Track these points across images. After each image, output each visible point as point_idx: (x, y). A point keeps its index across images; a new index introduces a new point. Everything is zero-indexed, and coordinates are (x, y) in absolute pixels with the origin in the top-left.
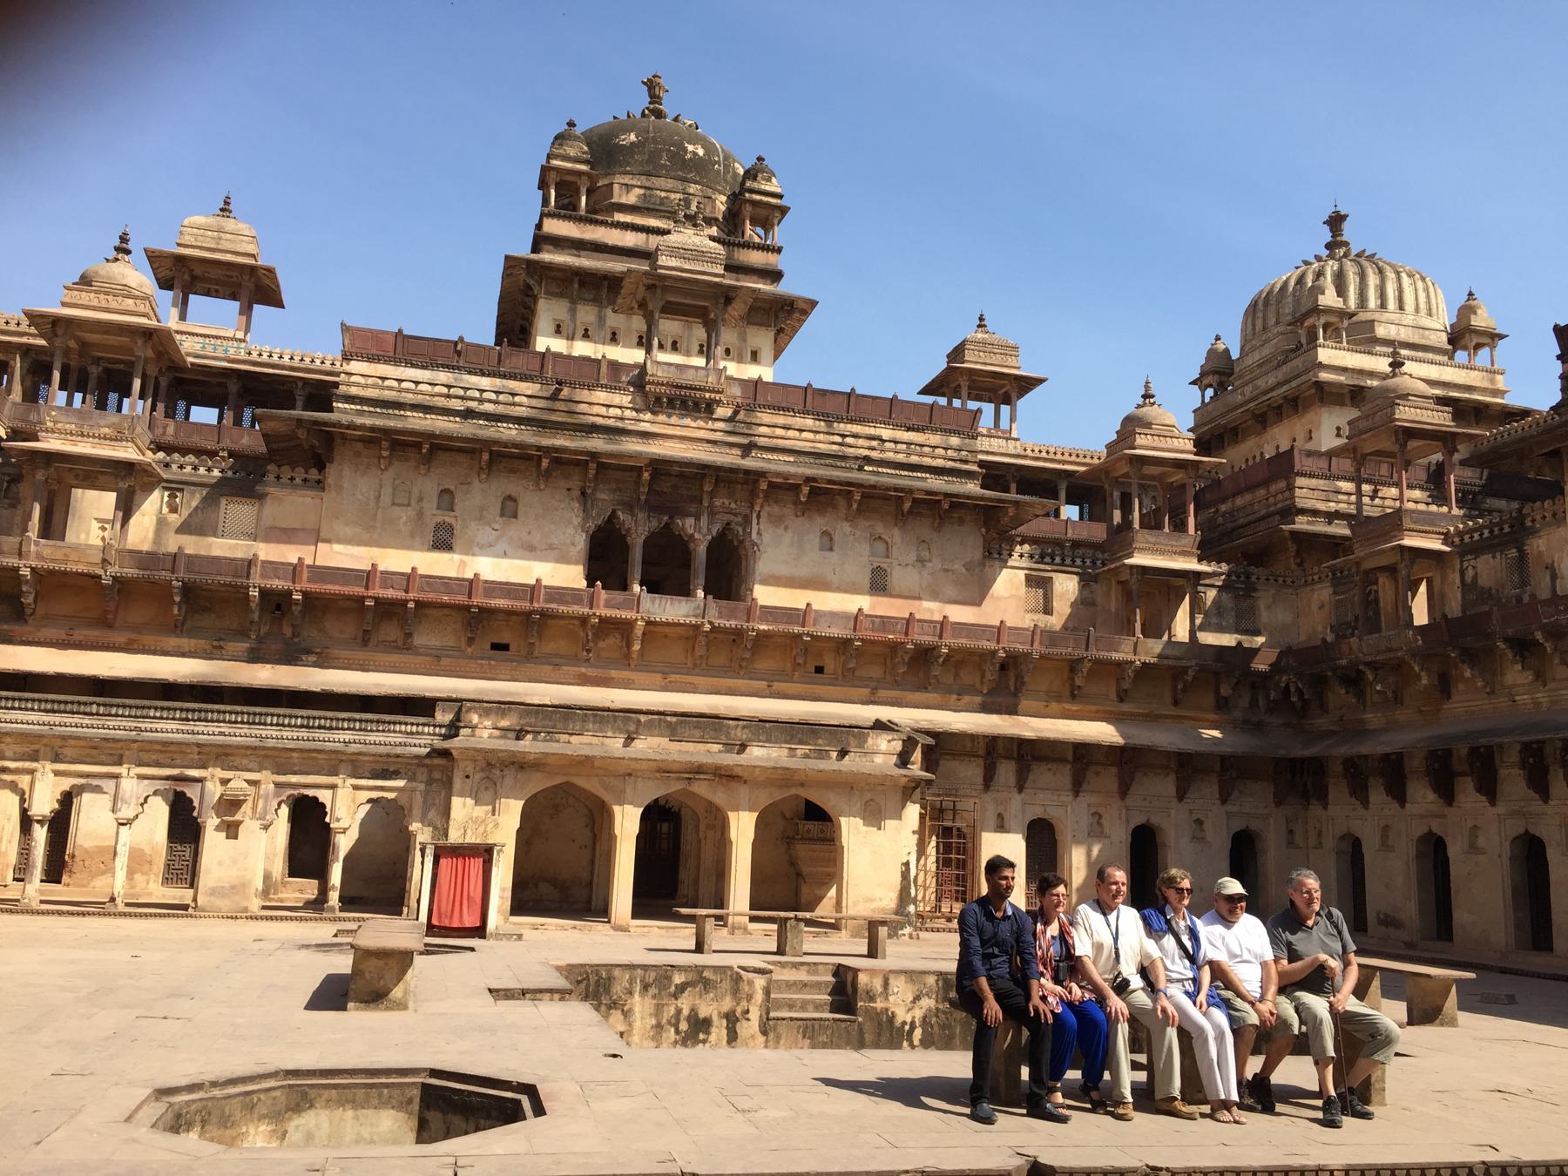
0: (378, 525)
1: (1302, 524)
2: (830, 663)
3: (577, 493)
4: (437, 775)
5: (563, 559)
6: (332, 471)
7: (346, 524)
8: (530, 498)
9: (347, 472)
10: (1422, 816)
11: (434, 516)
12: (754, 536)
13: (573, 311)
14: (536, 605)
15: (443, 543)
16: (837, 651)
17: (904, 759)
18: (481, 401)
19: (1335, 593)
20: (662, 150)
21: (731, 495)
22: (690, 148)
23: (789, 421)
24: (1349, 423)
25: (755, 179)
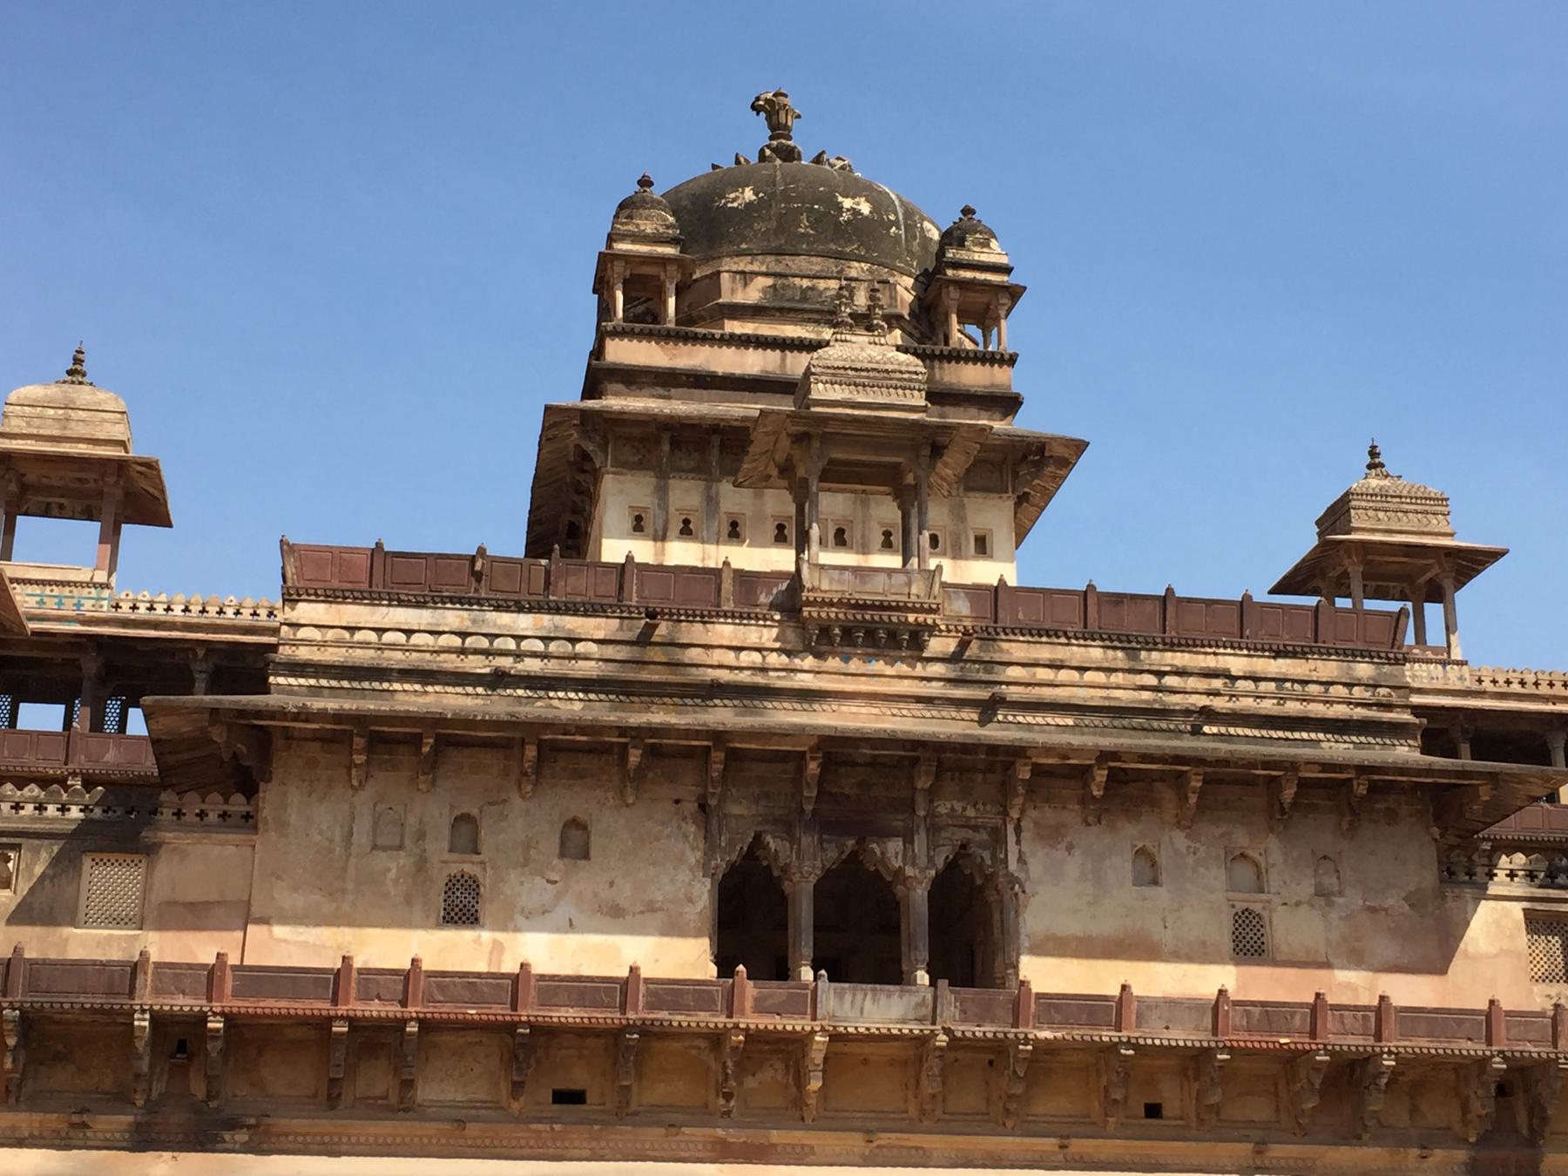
0: (350, 886)
3: (690, 807)
5: (674, 928)
6: (269, 795)
8: (611, 823)
9: (295, 797)
11: (445, 864)
12: (1013, 865)
13: (662, 492)
14: (631, 1015)
15: (461, 911)
18: (519, 655)
20: (799, 211)
22: (847, 203)
25: (961, 244)
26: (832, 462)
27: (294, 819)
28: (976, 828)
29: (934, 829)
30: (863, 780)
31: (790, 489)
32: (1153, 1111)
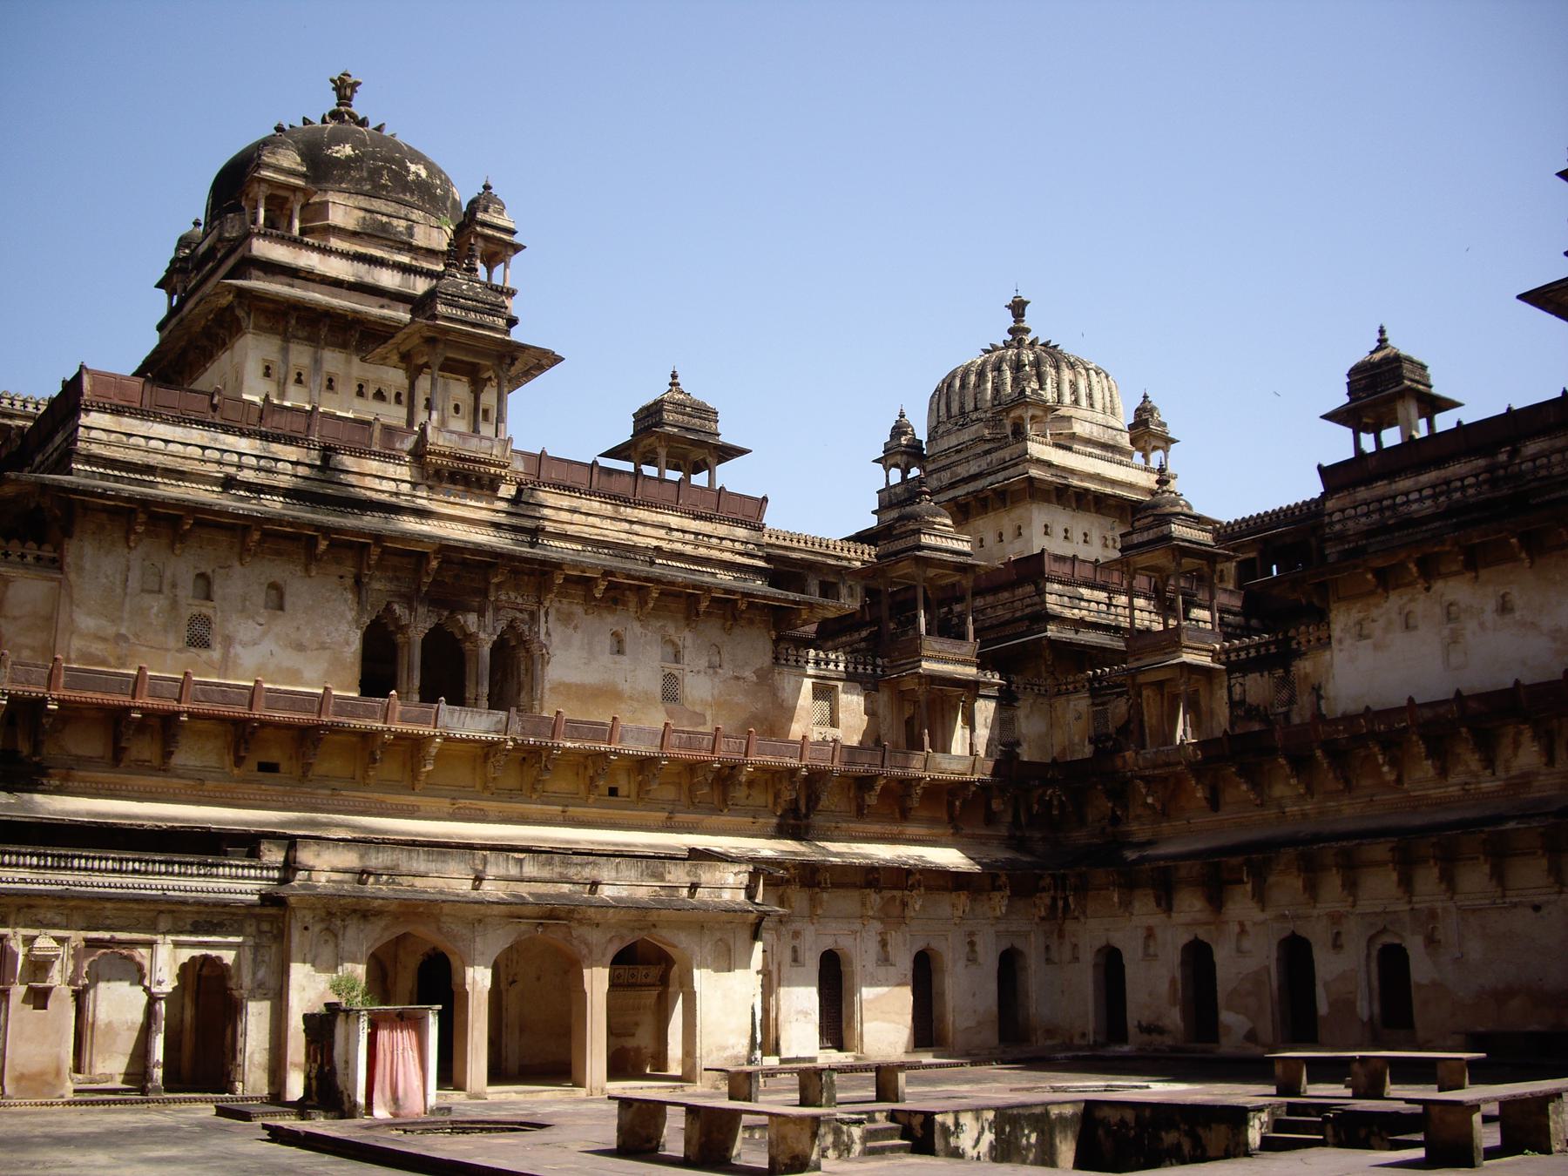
0: (126, 616)
1: (1052, 631)
2: (624, 785)
3: (349, 581)
4: (265, 927)
6: (71, 550)
7: (89, 614)
8: (300, 589)
9: (89, 549)
10: (1188, 925)
11: (191, 606)
12: (542, 637)
13: (285, 351)
14: (325, 719)
16: (629, 771)
17: (750, 892)
18: (240, 467)
19: (1093, 704)
20: (383, 168)
21: (517, 588)
22: (413, 168)
23: (576, 503)
24: (1122, 536)
25: (486, 210)
26: (447, 359)
27: (88, 566)
28: (521, 611)
29: (497, 609)
30: (464, 572)
31: (407, 370)
32: (613, 792)
